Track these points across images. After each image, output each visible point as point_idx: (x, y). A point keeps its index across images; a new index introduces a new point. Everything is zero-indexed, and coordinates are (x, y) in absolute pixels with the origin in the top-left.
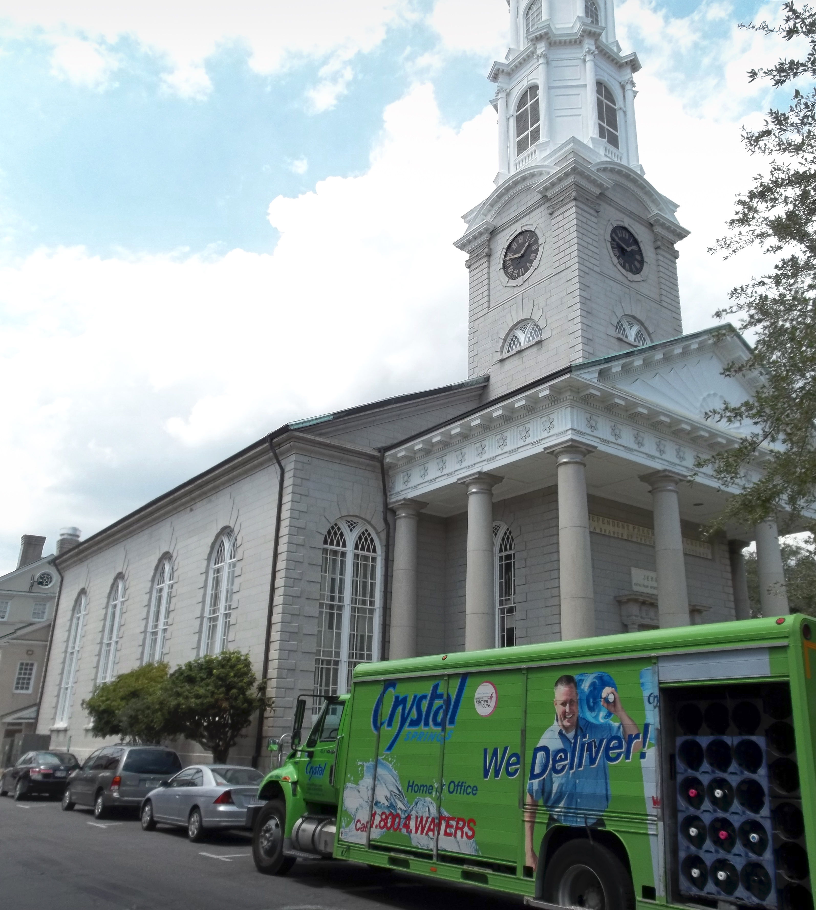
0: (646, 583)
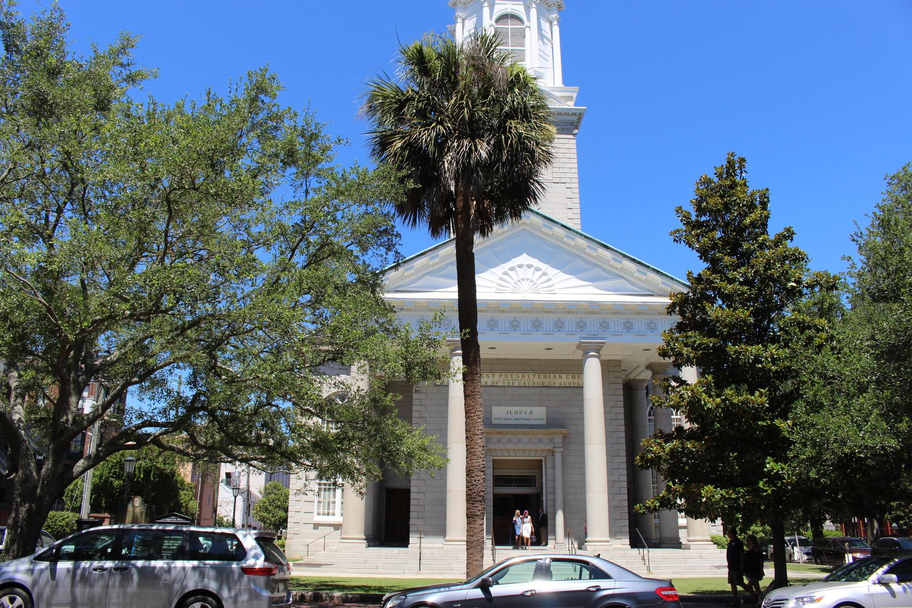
0: (509, 416)
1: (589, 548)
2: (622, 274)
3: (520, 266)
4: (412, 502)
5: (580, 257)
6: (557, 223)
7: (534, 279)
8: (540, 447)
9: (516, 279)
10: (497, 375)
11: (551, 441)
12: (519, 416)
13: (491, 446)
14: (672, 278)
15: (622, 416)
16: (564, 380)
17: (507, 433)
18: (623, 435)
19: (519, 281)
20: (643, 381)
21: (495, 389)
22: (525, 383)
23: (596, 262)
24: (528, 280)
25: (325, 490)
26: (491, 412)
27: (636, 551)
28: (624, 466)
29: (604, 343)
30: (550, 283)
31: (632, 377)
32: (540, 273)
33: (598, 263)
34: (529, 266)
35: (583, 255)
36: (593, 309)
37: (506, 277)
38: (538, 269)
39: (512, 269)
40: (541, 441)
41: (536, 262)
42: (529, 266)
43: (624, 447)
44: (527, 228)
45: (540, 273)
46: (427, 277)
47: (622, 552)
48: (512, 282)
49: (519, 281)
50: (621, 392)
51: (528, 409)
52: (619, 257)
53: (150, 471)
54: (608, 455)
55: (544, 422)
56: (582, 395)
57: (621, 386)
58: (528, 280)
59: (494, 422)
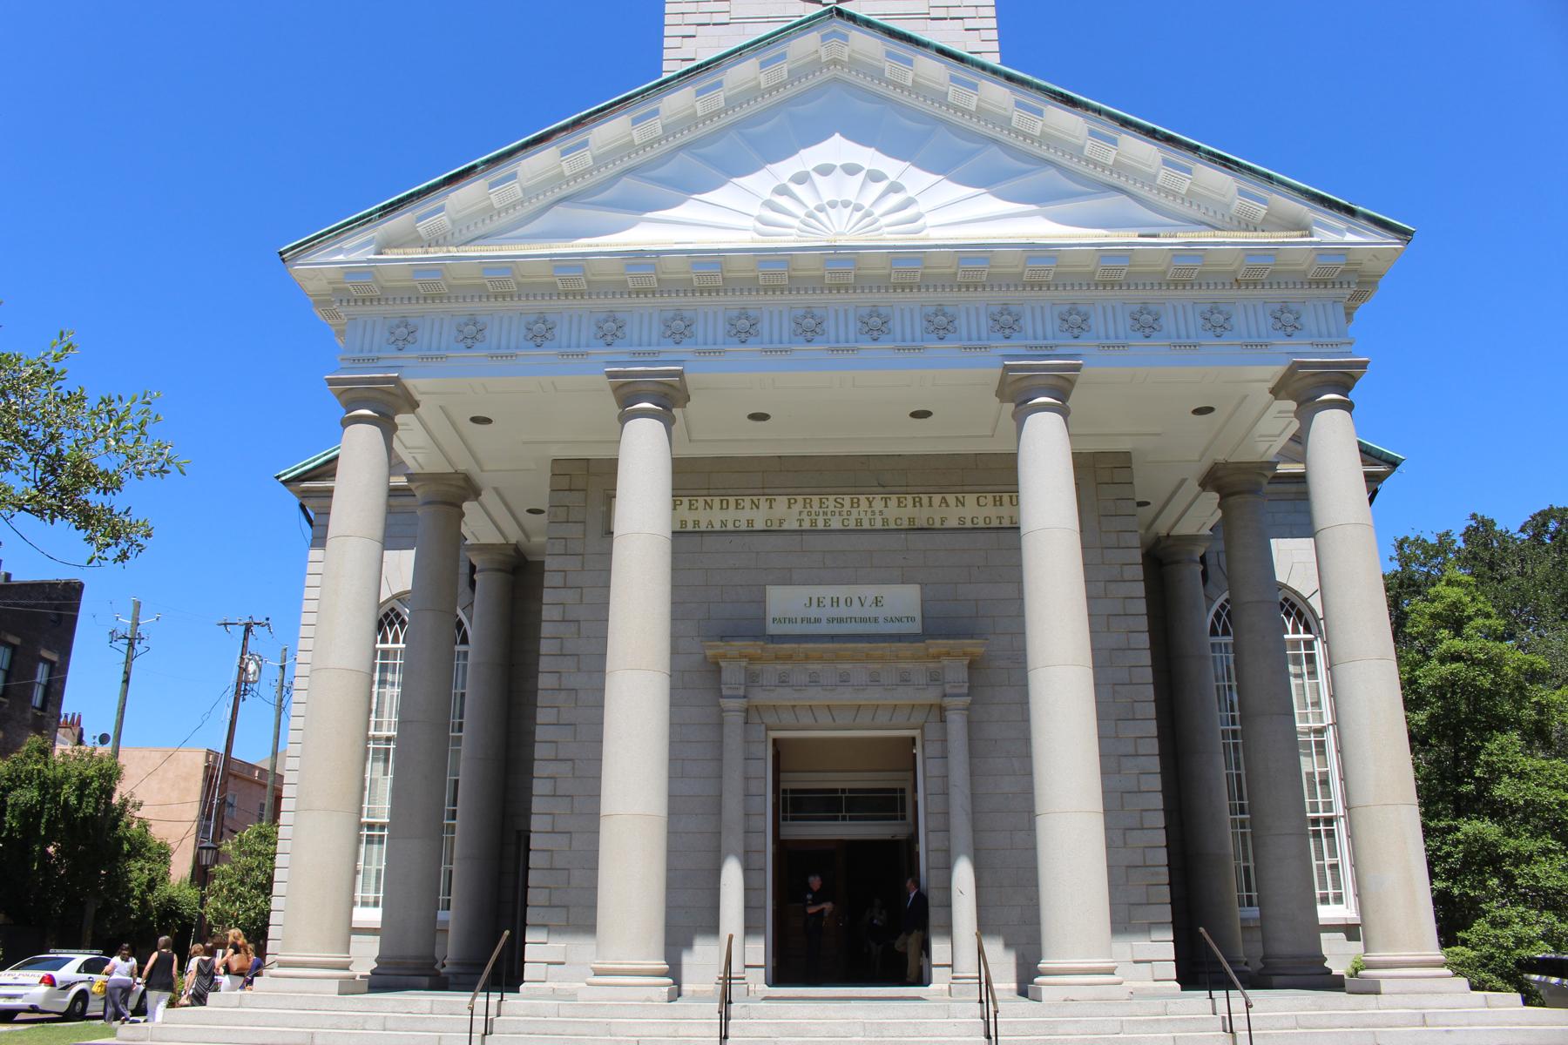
0: (814, 612)
1: (1046, 993)
2: (1121, 182)
3: (825, 170)
4: (534, 860)
5: (995, 141)
6: (926, 45)
7: (866, 202)
8: (904, 696)
9: (812, 205)
10: (782, 501)
11: (935, 678)
12: (843, 611)
13: (760, 697)
14: (1269, 177)
15: (1141, 607)
16: (973, 509)
17: (807, 658)
18: (1146, 658)
19: (821, 209)
20: (1193, 539)
21: (772, 539)
22: (859, 522)
23: (1042, 152)
24: (846, 204)
25: (370, 840)
26: (762, 602)
27: (1199, 998)
28: (1153, 746)
29: (1077, 368)
30: (910, 212)
31: (1162, 527)
32: (882, 186)
33: (1049, 154)
34: (852, 170)
35: (1003, 136)
36: (1038, 269)
37: (783, 201)
38: (876, 177)
39: (801, 178)
40: (905, 680)
41: (869, 158)
42: (852, 170)
43: (1150, 692)
44: (844, 74)
45: (881, 187)
46: (559, 209)
47: (1157, 1005)
48: (801, 213)
49: (821, 209)
50: (1138, 572)
51: (869, 592)
52: (1110, 129)
53: (39, 815)
54: (1102, 716)
55: (916, 628)
56: (1017, 549)
57: (1137, 556)
58: (846, 204)
59: (773, 629)
